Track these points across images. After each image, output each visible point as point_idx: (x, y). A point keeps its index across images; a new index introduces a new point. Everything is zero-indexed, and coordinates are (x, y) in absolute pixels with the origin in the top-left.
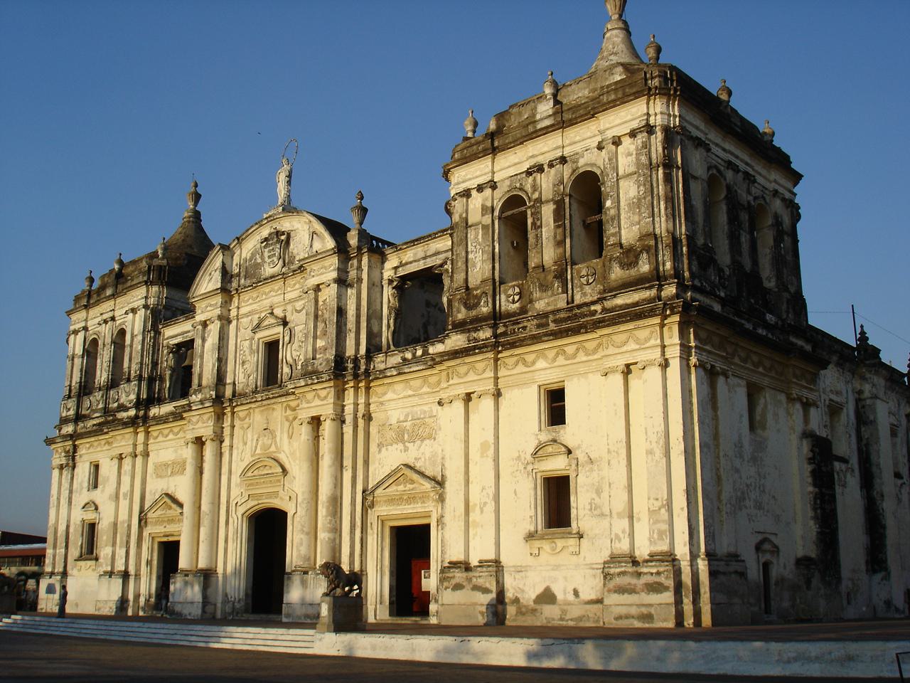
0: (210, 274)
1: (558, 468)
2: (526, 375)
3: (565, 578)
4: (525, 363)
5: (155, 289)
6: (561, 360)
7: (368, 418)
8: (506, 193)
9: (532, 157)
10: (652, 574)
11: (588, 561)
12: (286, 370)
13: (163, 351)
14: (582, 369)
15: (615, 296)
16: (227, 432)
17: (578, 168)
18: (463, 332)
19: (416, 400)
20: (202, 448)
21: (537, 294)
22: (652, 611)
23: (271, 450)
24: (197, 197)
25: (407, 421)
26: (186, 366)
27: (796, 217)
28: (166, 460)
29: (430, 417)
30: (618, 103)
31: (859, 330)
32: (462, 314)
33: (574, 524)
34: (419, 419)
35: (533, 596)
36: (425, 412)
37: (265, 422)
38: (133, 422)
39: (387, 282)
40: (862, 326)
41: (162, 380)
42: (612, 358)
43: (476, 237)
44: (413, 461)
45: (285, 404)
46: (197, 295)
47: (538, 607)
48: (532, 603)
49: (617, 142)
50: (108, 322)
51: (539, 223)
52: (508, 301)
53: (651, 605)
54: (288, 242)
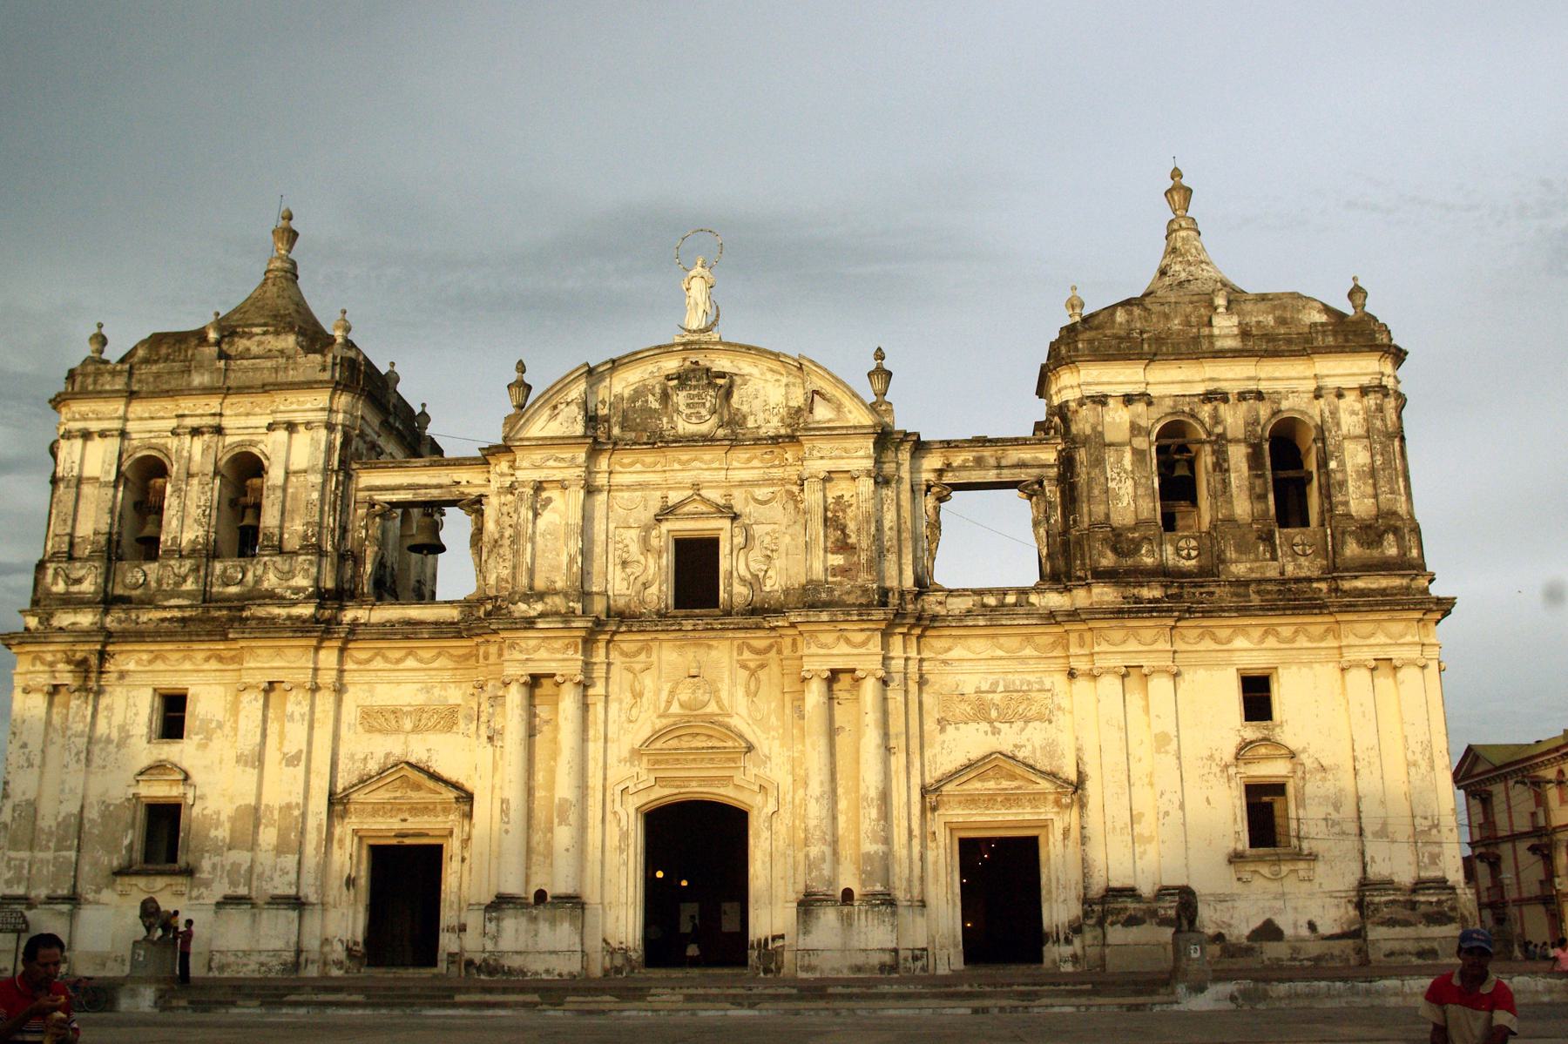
0: (555, 407)
1: (1277, 773)
2: (1220, 654)
3: (1295, 909)
4: (1216, 640)
5: (343, 400)
6: (1271, 642)
7: (922, 682)
8: (1167, 415)
9: (1212, 379)
10: (1431, 903)
11: (1326, 887)
14: (1305, 657)
15: (1356, 577)
16: (599, 672)
17: (1280, 411)
18: (1116, 584)
19: (1013, 665)
21: (1231, 554)
22: (1436, 945)
23: (708, 710)
25: (995, 692)
28: (401, 702)
29: (1039, 691)
32: (1108, 560)
34: (1018, 691)
35: (1246, 931)
36: (1029, 683)
38: (300, 628)
41: (358, 560)
42: (1355, 649)
43: (1120, 461)
44: (1011, 748)
46: (528, 435)
47: (1256, 945)
48: (1244, 941)
49: (1340, 394)
51: (1226, 466)
52: (1179, 555)
53: (1434, 939)
54: (728, 394)
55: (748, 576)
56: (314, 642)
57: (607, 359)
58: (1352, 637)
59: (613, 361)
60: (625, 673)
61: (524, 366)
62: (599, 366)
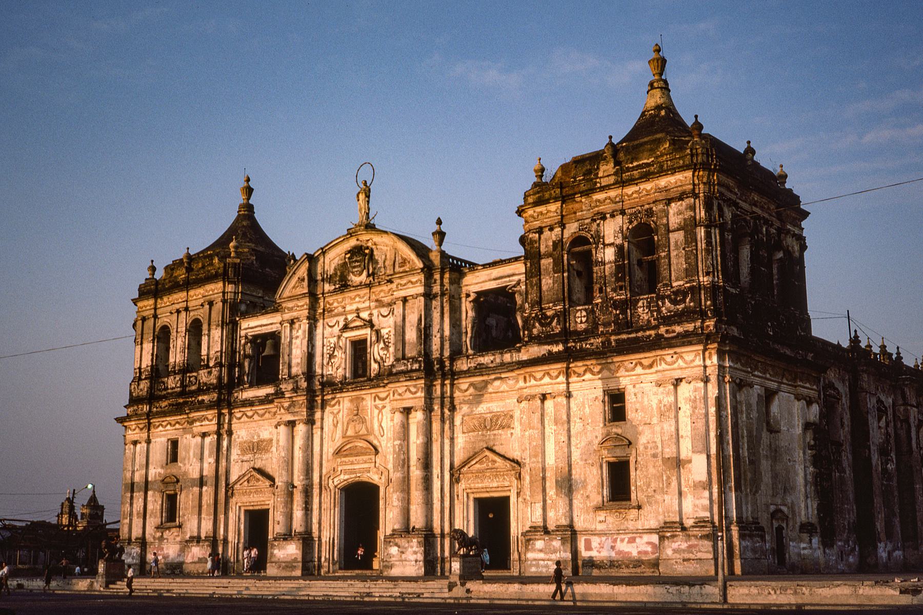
12: (374, 366)
13: (240, 341)
20: (293, 432)
24: (249, 191)
26: (265, 356)
27: (803, 247)
30: (670, 173)
31: (853, 334)
33: (633, 496)
37: (355, 409)
39: (465, 295)
40: (856, 331)
45: (373, 395)
50: (180, 312)
55: (379, 358)
56: (701, 347)
57: (319, 248)
58: (663, 364)
59: (322, 249)
60: (330, 415)
61: (441, 221)
62: (315, 253)
